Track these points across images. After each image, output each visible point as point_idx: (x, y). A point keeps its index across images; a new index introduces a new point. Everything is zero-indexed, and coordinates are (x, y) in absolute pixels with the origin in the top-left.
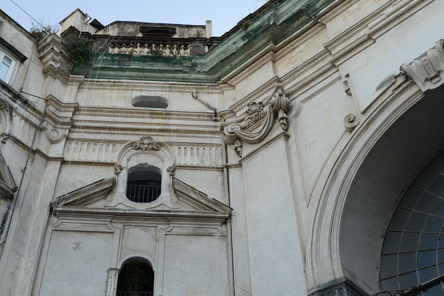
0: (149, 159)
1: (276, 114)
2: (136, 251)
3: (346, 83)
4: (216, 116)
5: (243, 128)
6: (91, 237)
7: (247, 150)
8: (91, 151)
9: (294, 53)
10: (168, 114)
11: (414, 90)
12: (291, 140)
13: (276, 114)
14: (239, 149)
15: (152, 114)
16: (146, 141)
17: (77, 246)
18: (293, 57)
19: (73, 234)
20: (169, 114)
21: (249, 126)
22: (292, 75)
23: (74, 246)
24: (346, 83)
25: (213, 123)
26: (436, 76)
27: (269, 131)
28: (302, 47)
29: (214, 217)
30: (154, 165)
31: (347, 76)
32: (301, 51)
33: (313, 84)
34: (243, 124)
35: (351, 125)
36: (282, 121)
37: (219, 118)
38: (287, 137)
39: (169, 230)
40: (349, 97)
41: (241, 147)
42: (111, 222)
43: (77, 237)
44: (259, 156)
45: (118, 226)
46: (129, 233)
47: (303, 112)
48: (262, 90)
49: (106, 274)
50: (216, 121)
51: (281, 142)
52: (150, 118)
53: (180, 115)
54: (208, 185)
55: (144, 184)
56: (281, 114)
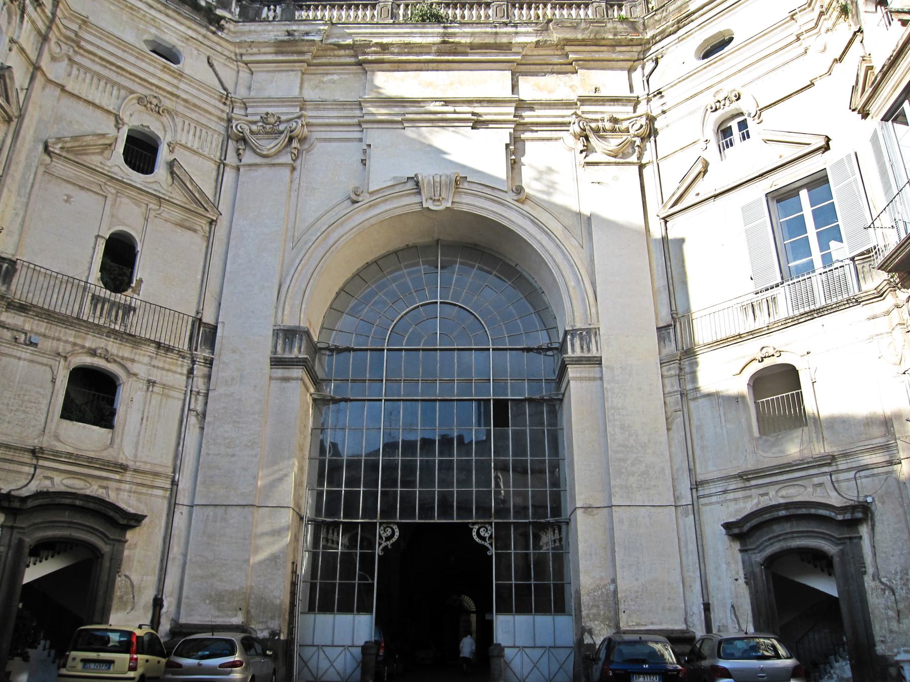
0: (153, 125)
1: (291, 139)
2: (124, 224)
3: (365, 151)
4: (226, 99)
5: (252, 132)
6: (83, 193)
7: (248, 157)
8: (94, 87)
9: (326, 79)
10: (180, 75)
11: (416, 199)
12: (296, 173)
13: (291, 139)
14: (241, 151)
15: (165, 67)
16: (155, 101)
17: (68, 200)
18: (324, 83)
19: (64, 184)
20: (182, 76)
21: (259, 133)
22: (320, 104)
23: (65, 198)
24: (365, 151)
25: (221, 106)
26: (439, 200)
27: (278, 153)
28: (335, 77)
29: (201, 210)
30: (156, 132)
31: (369, 146)
32: (334, 82)
33: (334, 129)
34: (254, 128)
35: (354, 197)
36: (294, 151)
37: (228, 103)
38: (294, 169)
39: (159, 212)
40: (361, 166)
41: (244, 150)
42: (105, 184)
43: (70, 189)
44: (260, 172)
45: (111, 190)
46: (121, 202)
47: (315, 151)
48: (283, 102)
49: (93, 239)
50: (225, 104)
51: (287, 172)
52: (162, 71)
53: (192, 80)
54: (201, 174)
55: (141, 152)
56: (295, 144)
